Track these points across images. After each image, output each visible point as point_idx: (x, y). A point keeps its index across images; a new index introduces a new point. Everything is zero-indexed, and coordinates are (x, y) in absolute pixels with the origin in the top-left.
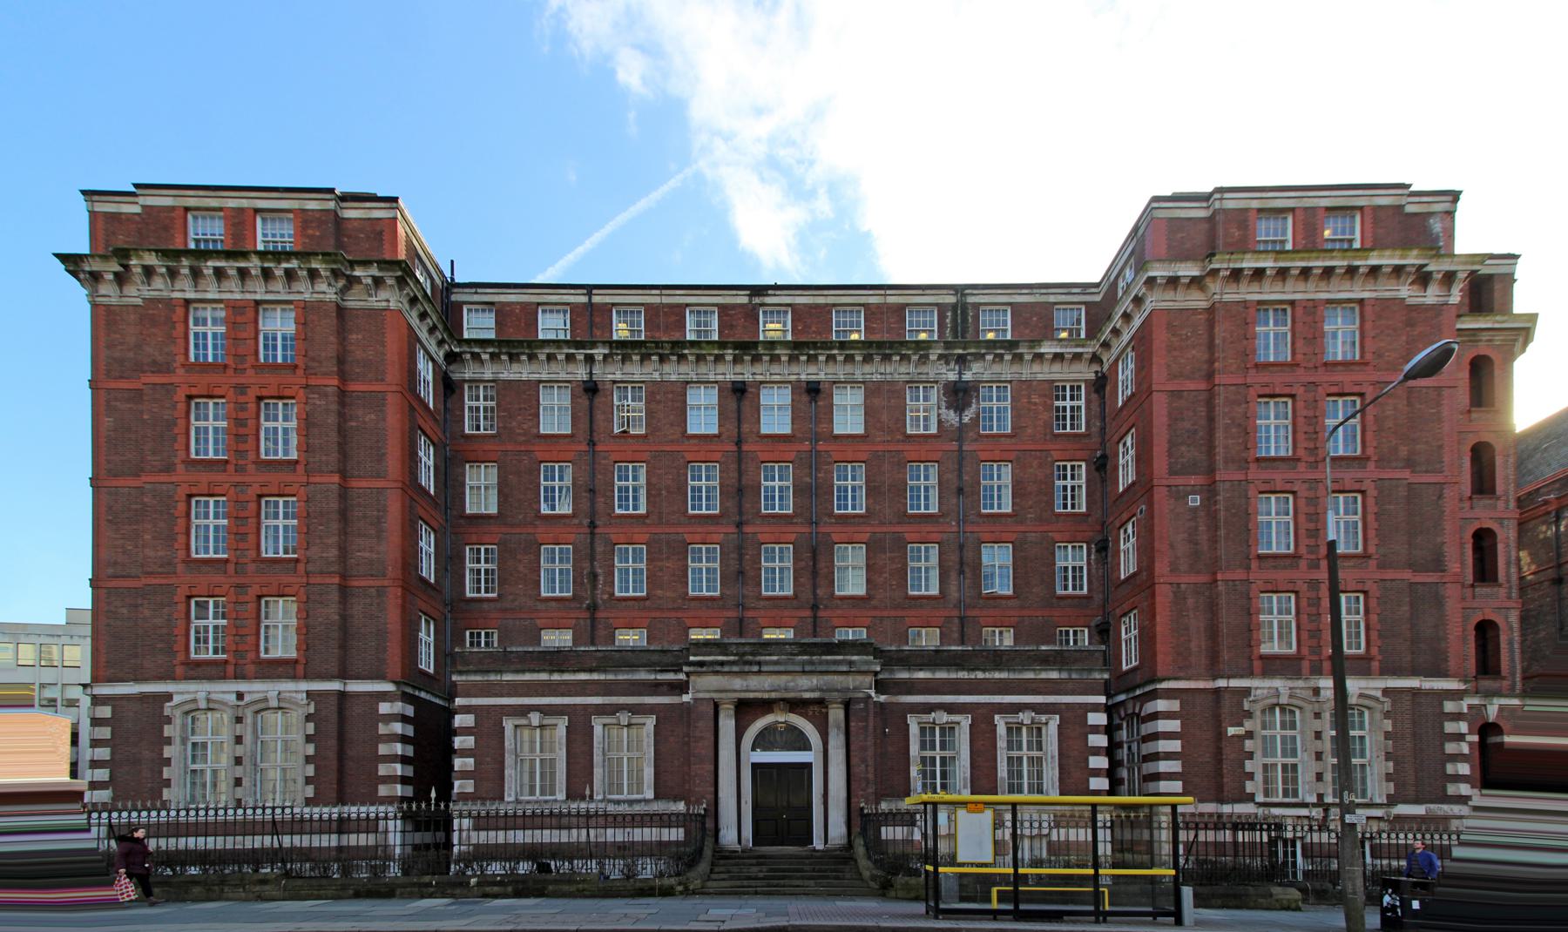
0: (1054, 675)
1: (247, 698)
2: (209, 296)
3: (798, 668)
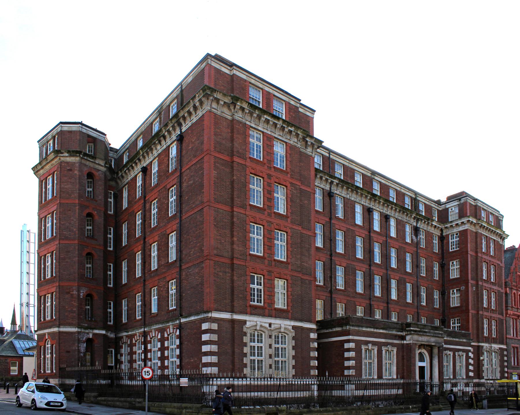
0: (465, 341)
1: (273, 326)
2: (260, 129)
3: (432, 335)
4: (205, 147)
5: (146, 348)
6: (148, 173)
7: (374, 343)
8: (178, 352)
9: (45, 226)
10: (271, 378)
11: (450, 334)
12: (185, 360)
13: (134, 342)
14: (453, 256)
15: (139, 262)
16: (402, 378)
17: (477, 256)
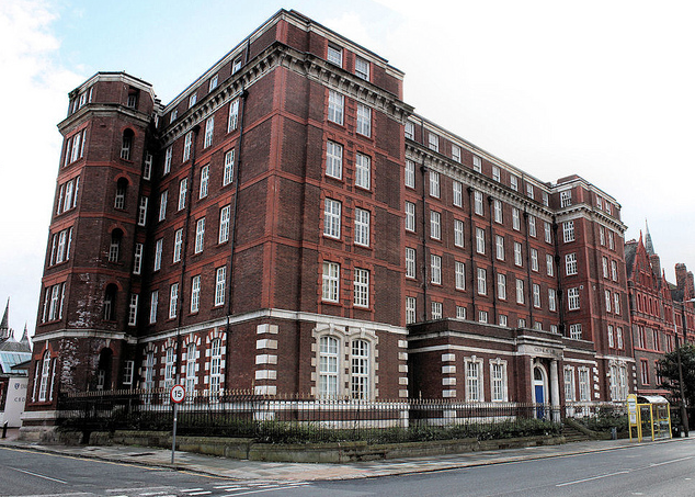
4: (275, 106)
5: (179, 358)
6: (201, 132)
7: (479, 355)
8: (223, 365)
9: (64, 195)
10: (347, 401)
11: (571, 344)
12: (233, 377)
13: (163, 350)
14: (569, 247)
15: (178, 243)
16: (516, 400)
17: (595, 250)
